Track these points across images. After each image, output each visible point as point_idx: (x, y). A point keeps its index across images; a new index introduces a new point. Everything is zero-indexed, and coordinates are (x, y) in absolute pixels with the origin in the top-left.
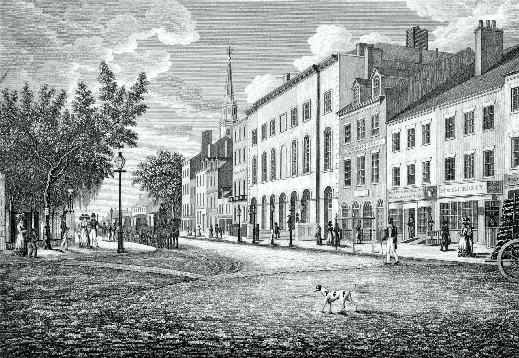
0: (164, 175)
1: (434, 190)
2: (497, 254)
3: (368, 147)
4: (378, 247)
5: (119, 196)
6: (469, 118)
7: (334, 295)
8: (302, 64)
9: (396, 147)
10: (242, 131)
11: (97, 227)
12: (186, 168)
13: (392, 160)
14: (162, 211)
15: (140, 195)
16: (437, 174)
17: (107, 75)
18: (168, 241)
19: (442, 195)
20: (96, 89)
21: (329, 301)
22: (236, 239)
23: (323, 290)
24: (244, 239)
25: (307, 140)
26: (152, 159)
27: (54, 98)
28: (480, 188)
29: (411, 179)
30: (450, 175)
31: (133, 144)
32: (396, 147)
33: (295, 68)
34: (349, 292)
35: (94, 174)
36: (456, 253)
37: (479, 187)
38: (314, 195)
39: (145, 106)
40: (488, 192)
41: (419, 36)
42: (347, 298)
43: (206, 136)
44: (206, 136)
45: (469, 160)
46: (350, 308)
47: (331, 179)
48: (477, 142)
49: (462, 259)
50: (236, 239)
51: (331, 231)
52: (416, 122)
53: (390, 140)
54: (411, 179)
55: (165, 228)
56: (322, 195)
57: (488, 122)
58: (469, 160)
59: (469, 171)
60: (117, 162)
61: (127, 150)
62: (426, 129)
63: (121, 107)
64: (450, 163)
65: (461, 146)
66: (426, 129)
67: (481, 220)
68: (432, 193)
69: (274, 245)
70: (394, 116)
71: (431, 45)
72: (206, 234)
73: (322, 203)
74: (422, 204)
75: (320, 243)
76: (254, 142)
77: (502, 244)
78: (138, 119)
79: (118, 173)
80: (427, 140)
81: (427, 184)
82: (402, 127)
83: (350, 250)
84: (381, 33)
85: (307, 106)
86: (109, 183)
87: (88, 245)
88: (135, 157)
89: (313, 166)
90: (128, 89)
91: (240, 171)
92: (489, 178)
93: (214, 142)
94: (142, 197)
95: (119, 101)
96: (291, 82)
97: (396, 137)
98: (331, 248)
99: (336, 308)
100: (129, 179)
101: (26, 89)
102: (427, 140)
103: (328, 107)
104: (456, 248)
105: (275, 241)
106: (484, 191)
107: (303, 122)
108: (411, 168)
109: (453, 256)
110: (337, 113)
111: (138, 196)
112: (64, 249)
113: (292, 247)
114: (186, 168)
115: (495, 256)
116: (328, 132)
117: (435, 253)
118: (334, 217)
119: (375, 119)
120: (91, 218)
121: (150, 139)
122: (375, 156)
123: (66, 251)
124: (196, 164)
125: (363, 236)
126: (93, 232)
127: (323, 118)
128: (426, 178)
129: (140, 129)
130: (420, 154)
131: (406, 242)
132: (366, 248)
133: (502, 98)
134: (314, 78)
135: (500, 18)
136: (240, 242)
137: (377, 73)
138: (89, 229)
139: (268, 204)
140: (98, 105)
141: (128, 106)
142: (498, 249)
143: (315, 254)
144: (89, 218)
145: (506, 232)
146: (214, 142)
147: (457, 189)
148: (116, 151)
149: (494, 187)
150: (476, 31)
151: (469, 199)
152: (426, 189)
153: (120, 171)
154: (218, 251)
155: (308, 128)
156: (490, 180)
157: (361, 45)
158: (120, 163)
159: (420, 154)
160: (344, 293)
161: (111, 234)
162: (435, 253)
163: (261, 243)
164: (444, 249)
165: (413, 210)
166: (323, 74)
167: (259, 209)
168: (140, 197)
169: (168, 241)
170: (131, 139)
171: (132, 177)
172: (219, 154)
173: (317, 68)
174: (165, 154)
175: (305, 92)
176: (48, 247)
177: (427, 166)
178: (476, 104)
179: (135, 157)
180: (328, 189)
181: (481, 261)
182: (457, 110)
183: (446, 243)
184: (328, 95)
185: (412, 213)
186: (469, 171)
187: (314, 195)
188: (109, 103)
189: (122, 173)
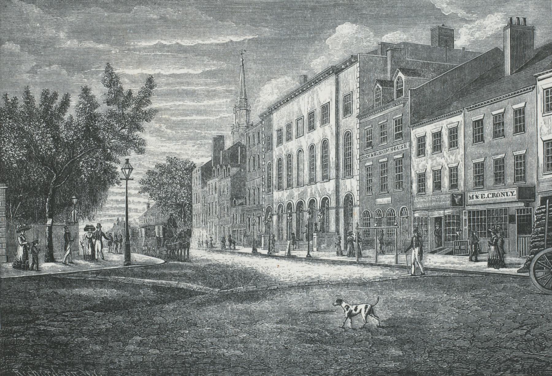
0: (171, 185)
1: (463, 195)
2: (529, 264)
4: (403, 258)
5: (126, 204)
8: (318, 64)
9: (421, 152)
11: (103, 239)
12: (196, 174)
13: (418, 165)
14: (172, 222)
16: (466, 177)
17: (112, 81)
18: (178, 252)
19: (470, 201)
20: (99, 91)
21: (350, 315)
22: (250, 250)
23: (344, 304)
24: (259, 250)
25: (325, 144)
26: (159, 166)
28: (511, 194)
29: (438, 186)
31: (141, 152)
32: (421, 152)
33: (311, 70)
34: (372, 306)
35: (94, 191)
37: (509, 193)
38: (333, 204)
39: (156, 111)
40: (519, 198)
42: (369, 313)
43: (219, 140)
44: (219, 140)
45: (500, 165)
47: (351, 185)
48: (508, 147)
49: (492, 270)
50: (250, 250)
51: (352, 241)
52: (443, 125)
53: (414, 143)
54: (438, 186)
55: (172, 237)
57: (520, 126)
58: (500, 165)
59: (499, 178)
60: (123, 170)
61: (133, 155)
64: (479, 168)
65: (488, 153)
66: (453, 133)
67: (513, 228)
68: (458, 201)
69: (290, 257)
71: (459, 43)
72: (218, 245)
73: (342, 211)
74: (448, 212)
76: (269, 147)
77: (536, 253)
78: (144, 124)
79: (125, 181)
80: (453, 144)
81: (455, 191)
82: (427, 130)
83: (373, 262)
86: (115, 192)
87: (92, 258)
88: (142, 164)
90: (135, 94)
91: (254, 181)
92: (522, 183)
94: (151, 206)
95: (124, 105)
96: (308, 84)
97: (421, 140)
99: (359, 323)
102: (453, 144)
103: (347, 110)
104: (486, 258)
105: (293, 253)
106: (515, 197)
107: (277, 146)
108: (437, 175)
109: (483, 266)
110: (358, 117)
111: (146, 206)
112: (67, 261)
113: (309, 259)
114: (196, 174)
116: (348, 135)
117: (460, 262)
118: (355, 226)
120: (96, 229)
121: (158, 146)
122: (399, 161)
123: (70, 264)
124: (207, 171)
125: (386, 245)
128: (454, 185)
129: (148, 135)
130: (447, 159)
131: (433, 252)
132: (388, 259)
133: (534, 102)
134: (332, 80)
135: (531, 14)
136: (255, 253)
137: (400, 74)
138: (94, 240)
139: (332, 208)
140: (102, 109)
141: (131, 111)
142: (531, 260)
143: (321, 264)
144: (94, 229)
145: (338, 231)
146: (226, 149)
147: (486, 196)
148: (122, 159)
149: (526, 194)
150: (505, 29)
151: (503, 206)
152: (453, 197)
154: (220, 261)
156: (523, 186)
158: (127, 171)
159: (447, 159)
161: (117, 246)
162: (460, 262)
163: (276, 254)
164: (474, 258)
166: (342, 75)
167: (332, 213)
168: (148, 207)
169: (178, 252)
171: (139, 186)
172: (230, 158)
173: (336, 70)
174: (172, 161)
175: (325, 92)
176: (51, 258)
177: (453, 172)
178: (508, 107)
179: (142, 164)
180: (349, 199)
182: (485, 113)
183: (475, 256)
184: (348, 97)
185: (438, 220)
186: (499, 178)
187: (333, 204)
188: (114, 108)
189: (129, 181)
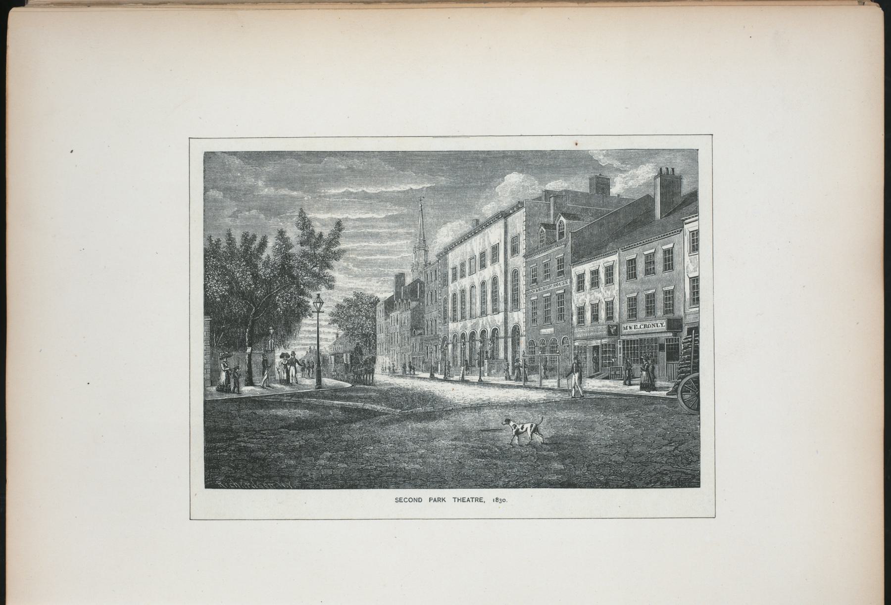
0: (357, 316)
1: (618, 326)
3: (555, 287)
6: (650, 261)
7: (522, 428)
8: (489, 209)
9: (580, 287)
10: (433, 273)
11: (297, 365)
12: (380, 308)
15: (337, 334)
17: (305, 224)
19: (624, 331)
20: (293, 234)
22: (428, 375)
23: (512, 423)
24: (436, 375)
25: (495, 280)
27: (256, 244)
29: (595, 318)
30: (633, 315)
31: (331, 287)
36: (638, 387)
38: (502, 334)
41: (602, 185)
43: (400, 277)
45: (651, 299)
46: (538, 439)
47: (518, 317)
50: (428, 375)
51: (519, 367)
53: (575, 280)
54: (595, 318)
55: (359, 364)
56: (510, 333)
57: (669, 265)
58: (651, 299)
59: (650, 310)
62: (609, 271)
63: (320, 251)
64: (633, 302)
67: (663, 355)
68: (614, 332)
69: (463, 381)
70: (579, 256)
71: (615, 190)
73: (510, 340)
74: (604, 341)
75: (508, 378)
78: (334, 263)
80: (609, 280)
82: (586, 268)
84: (526, 322)
85: (495, 249)
86: (307, 324)
87: (287, 382)
89: (502, 306)
90: (325, 236)
92: (670, 316)
93: (406, 285)
95: (316, 246)
96: (480, 227)
97: (581, 277)
98: (517, 384)
99: (525, 440)
100: (326, 321)
101: (229, 235)
102: (609, 280)
103: (515, 251)
105: (466, 378)
106: (664, 328)
111: (335, 336)
115: (675, 391)
116: (516, 273)
118: (521, 353)
119: (561, 261)
121: (346, 282)
124: (390, 305)
126: (292, 369)
127: (510, 260)
128: (610, 318)
129: (336, 273)
130: (603, 294)
131: (591, 377)
134: (501, 223)
136: (432, 378)
141: (322, 251)
142: (678, 384)
146: (406, 285)
151: (654, 336)
152: (609, 328)
153: (318, 312)
155: (495, 270)
157: (547, 193)
159: (603, 294)
160: (531, 426)
164: (627, 382)
165: (598, 347)
167: (501, 341)
170: (330, 284)
172: (410, 293)
173: (504, 215)
178: (658, 248)
181: (663, 394)
184: (515, 239)
186: (650, 310)
187: (502, 334)
188: (306, 248)
